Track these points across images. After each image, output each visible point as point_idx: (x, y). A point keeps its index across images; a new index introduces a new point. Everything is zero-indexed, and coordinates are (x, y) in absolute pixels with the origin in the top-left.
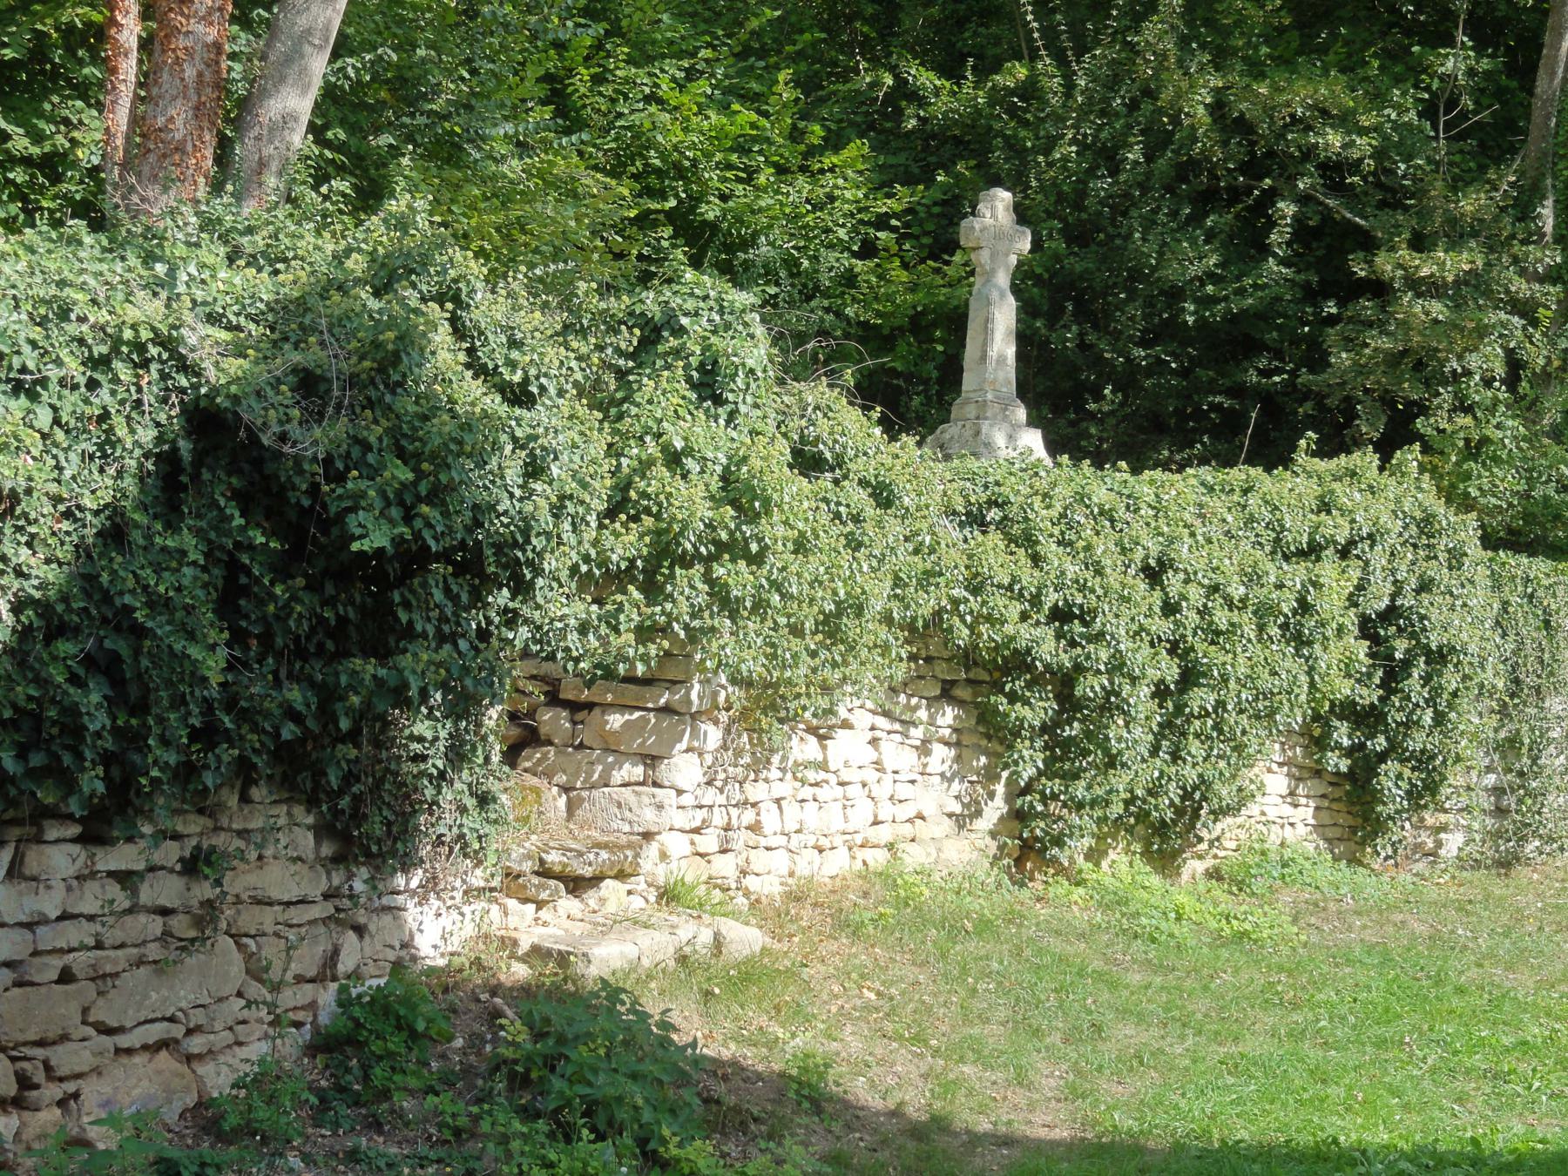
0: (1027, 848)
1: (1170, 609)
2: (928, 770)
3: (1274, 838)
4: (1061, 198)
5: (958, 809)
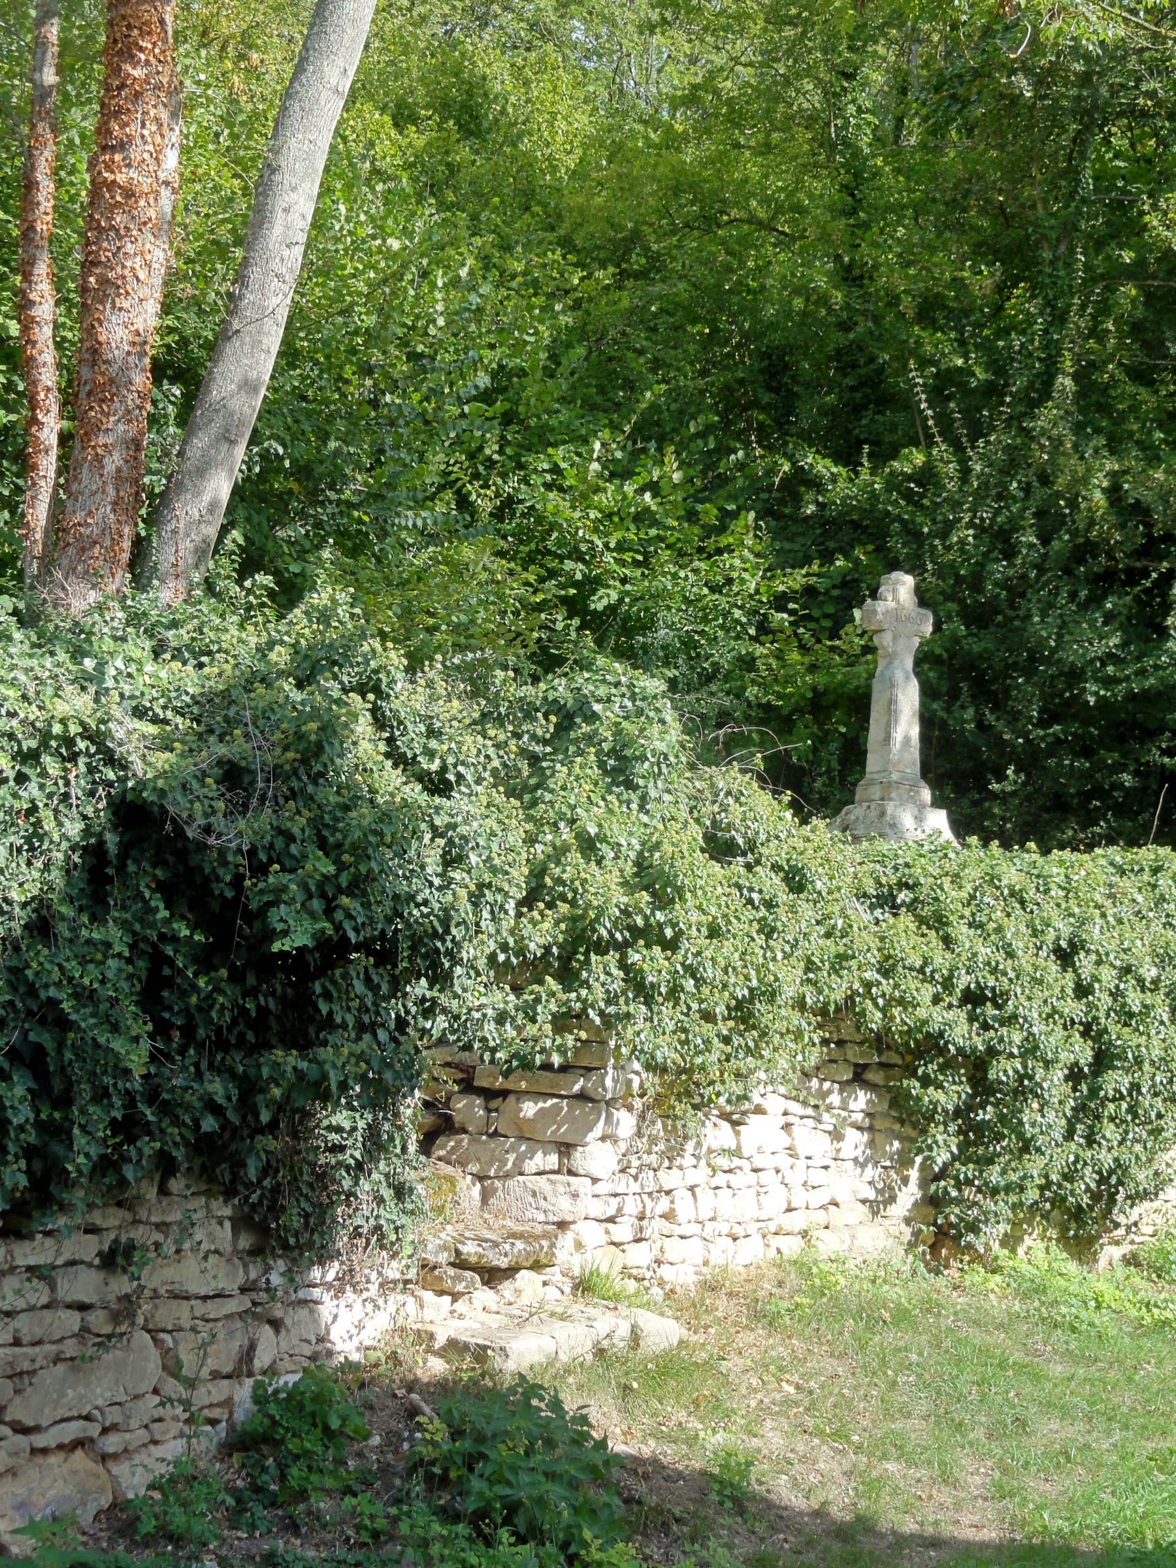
0: (943, 1234)
1: (1082, 991)
5: (872, 1195)
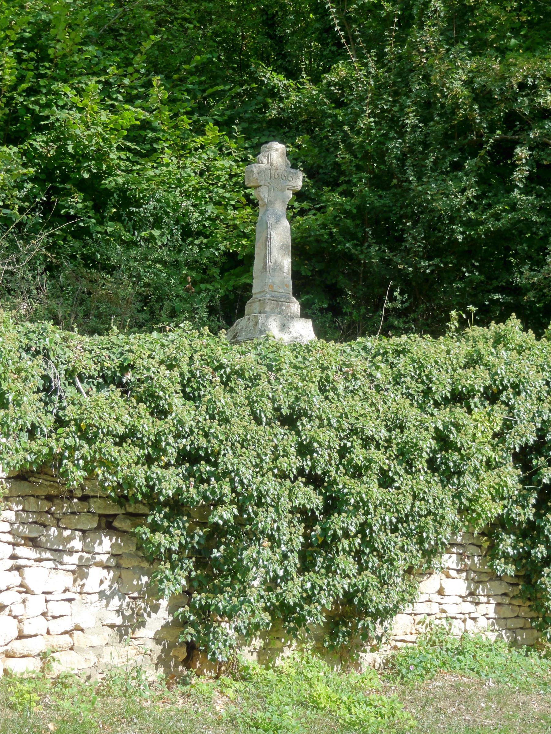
0: (188, 652)
1: (304, 450)
2: (85, 590)
3: (457, 628)
4: (367, 156)
5: (119, 621)
